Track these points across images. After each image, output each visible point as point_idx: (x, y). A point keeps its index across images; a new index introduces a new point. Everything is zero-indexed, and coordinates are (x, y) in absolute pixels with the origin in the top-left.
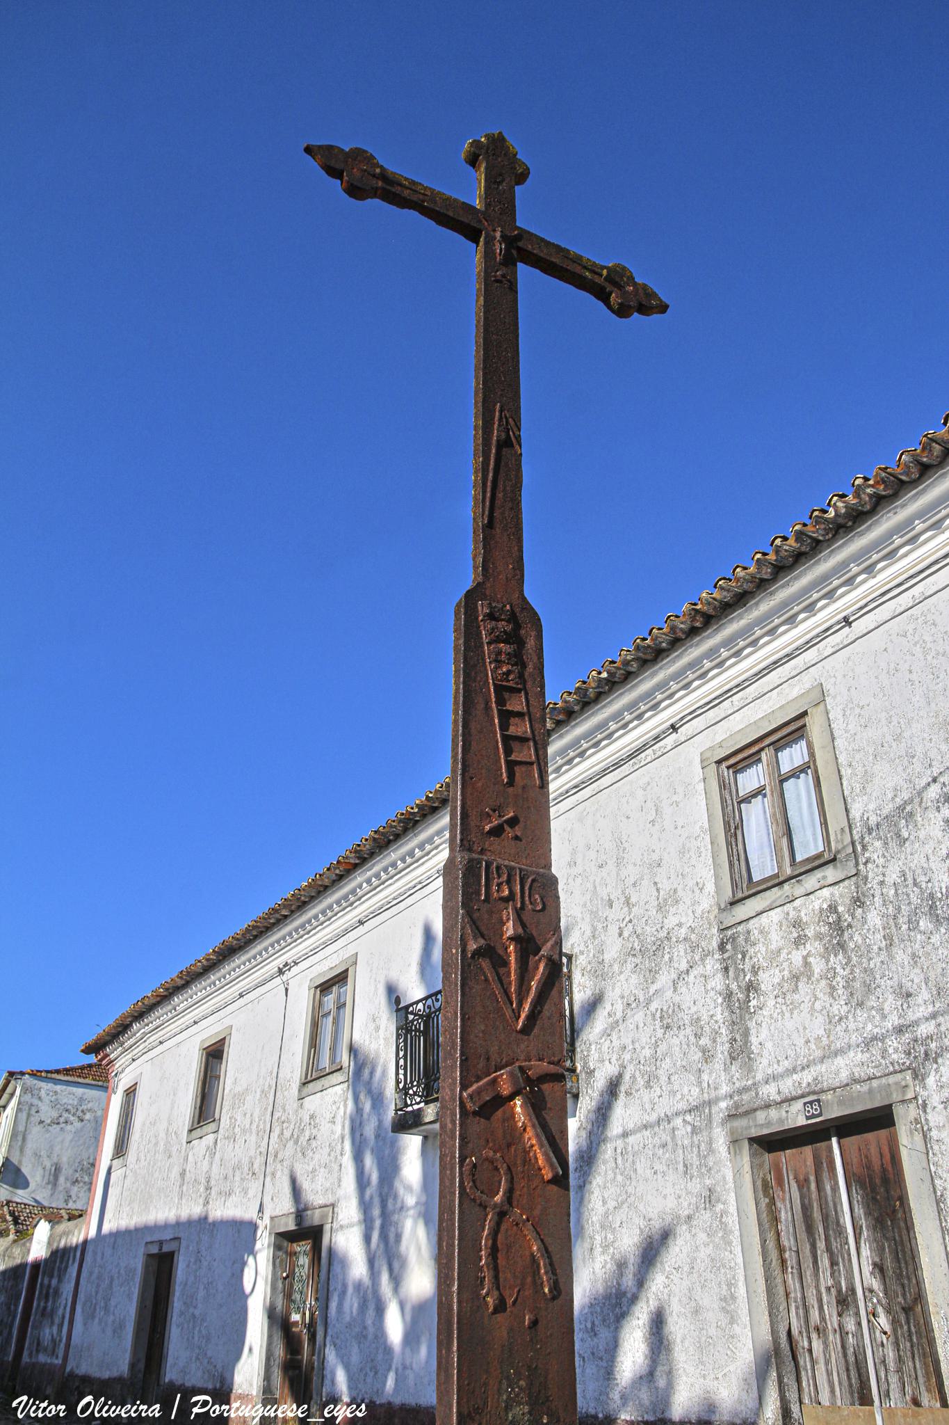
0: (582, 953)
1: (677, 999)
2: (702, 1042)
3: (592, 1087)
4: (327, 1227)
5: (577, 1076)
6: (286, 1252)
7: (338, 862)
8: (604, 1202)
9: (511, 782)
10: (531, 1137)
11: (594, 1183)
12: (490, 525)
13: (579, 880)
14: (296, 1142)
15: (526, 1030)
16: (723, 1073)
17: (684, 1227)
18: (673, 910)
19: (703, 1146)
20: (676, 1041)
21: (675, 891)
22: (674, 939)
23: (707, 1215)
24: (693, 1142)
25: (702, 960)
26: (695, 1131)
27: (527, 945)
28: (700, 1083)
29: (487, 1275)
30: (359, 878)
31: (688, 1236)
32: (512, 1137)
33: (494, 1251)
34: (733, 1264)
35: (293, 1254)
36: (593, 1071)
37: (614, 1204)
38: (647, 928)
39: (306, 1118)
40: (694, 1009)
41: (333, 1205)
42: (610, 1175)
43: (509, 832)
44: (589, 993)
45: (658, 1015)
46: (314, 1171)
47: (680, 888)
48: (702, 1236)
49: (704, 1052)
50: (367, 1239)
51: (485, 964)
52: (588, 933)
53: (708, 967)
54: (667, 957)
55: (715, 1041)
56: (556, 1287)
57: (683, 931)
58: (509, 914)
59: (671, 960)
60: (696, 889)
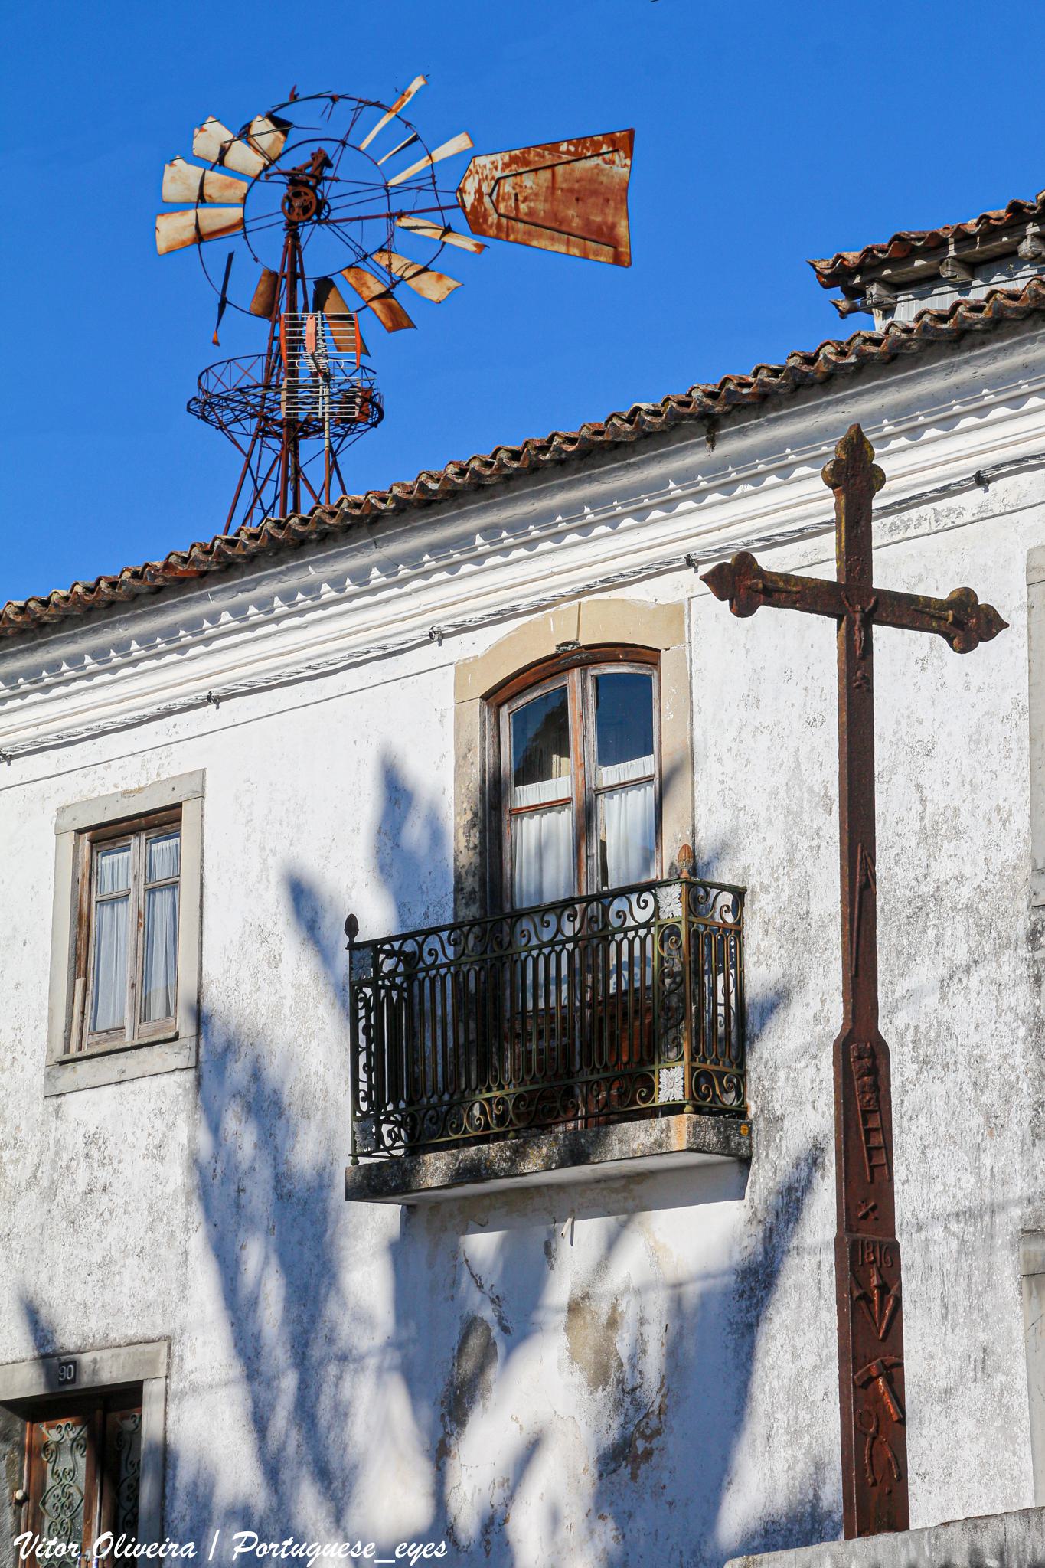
0: (765, 889)
1: (945, 1014)
2: (987, 1098)
3: (778, 1148)
4: (152, 1390)
5: (750, 1124)
6: (20, 1446)
7: (167, 566)
8: (795, 1356)
9: (872, 1182)
10: (887, 1398)
11: (777, 1321)
12: (856, 975)
13: (764, 740)
14: (50, 1195)
15: (884, 1339)
16: (1018, 1159)
17: (938, 1408)
18: (948, 847)
19: (976, 1277)
20: (938, 1089)
21: (956, 810)
22: (947, 903)
23: (977, 1391)
24: (959, 1268)
25: (997, 954)
26: (964, 1249)
27: (884, 1289)
28: (977, 1169)
29: (869, 1468)
30: (216, 601)
31: (944, 1423)
32: (878, 1398)
33: (871, 1457)
34: (1016, 1473)
35: (38, 1452)
36: (782, 1118)
37: (813, 1360)
38: (897, 869)
39: (76, 1142)
40: (975, 1039)
41: (168, 1340)
42: (808, 1308)
43: (872, 1216)
44: (777, 971)
45: (909, 1036)
46: (106, 1263)
47: (965, 808)
48: (967, 1425)
49: (988, 1118)
50: (260, 1422)
51: (863, 1303)
52: (780, 852)
53: (1006, 969)
54: (931, 933)
55: (1007, 1102)
56: (899, 1475)
57: (965, 892)
58: (874, 1271)
59: (939, 939)
60: (995, 818)
